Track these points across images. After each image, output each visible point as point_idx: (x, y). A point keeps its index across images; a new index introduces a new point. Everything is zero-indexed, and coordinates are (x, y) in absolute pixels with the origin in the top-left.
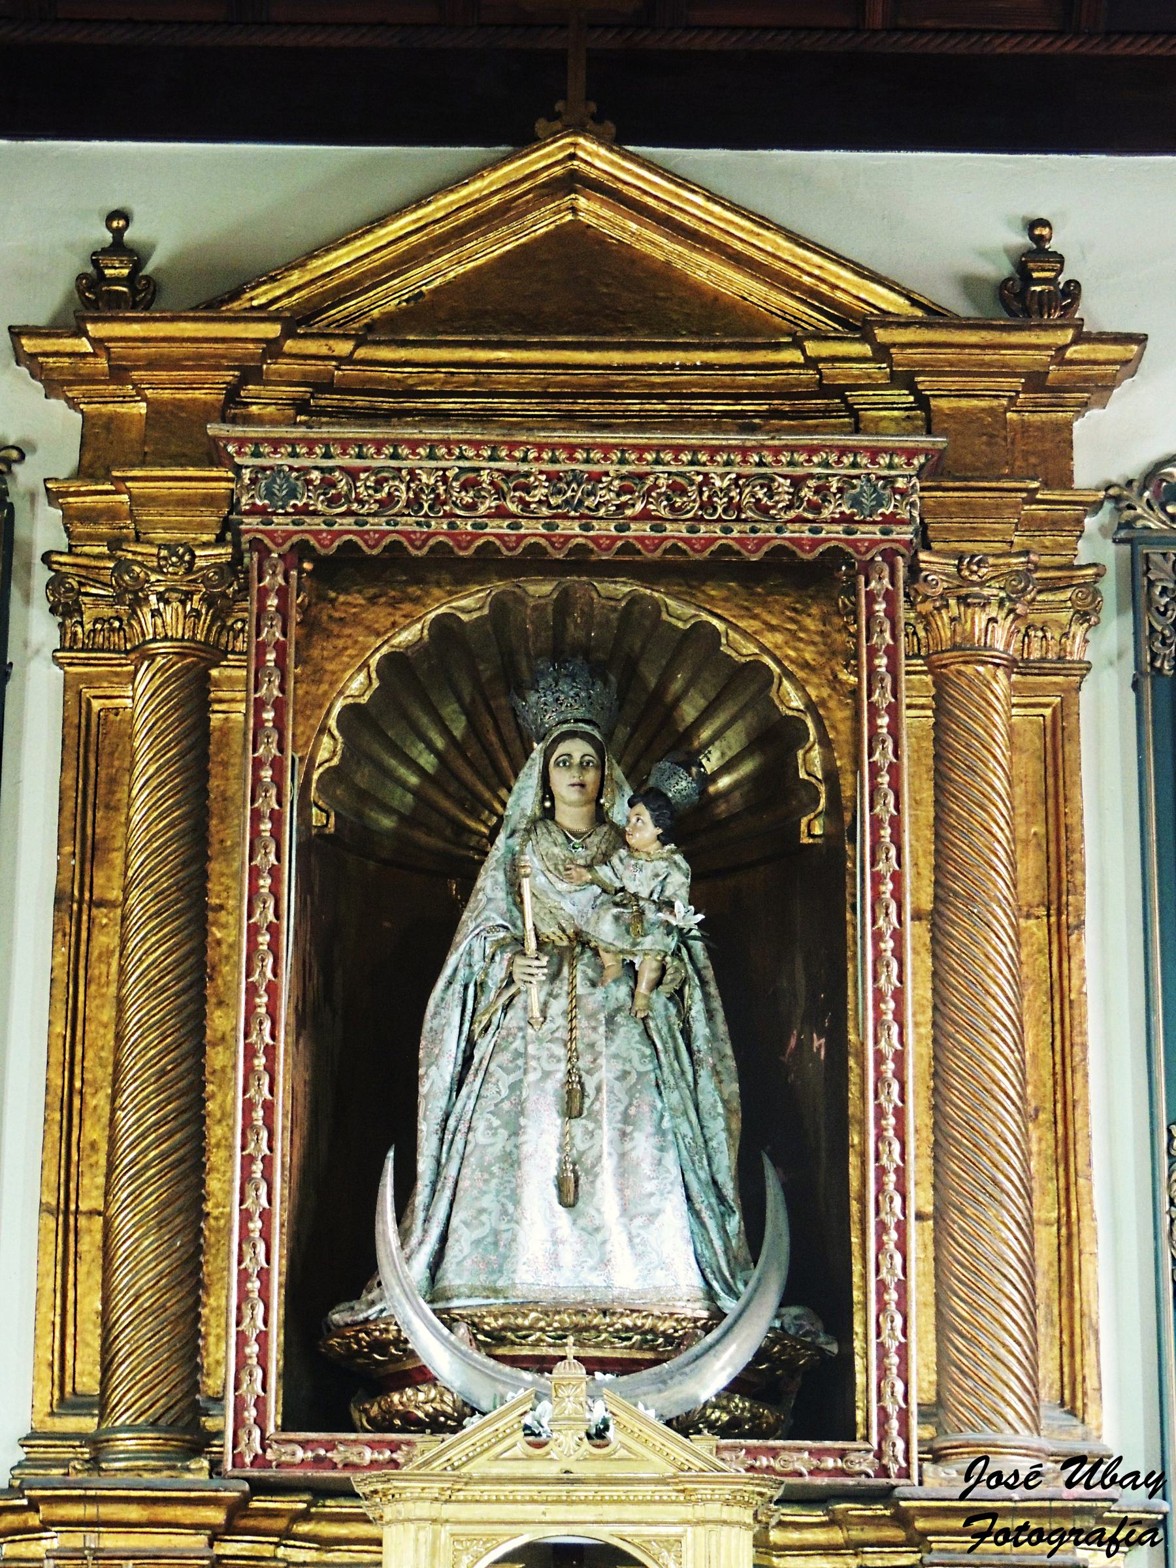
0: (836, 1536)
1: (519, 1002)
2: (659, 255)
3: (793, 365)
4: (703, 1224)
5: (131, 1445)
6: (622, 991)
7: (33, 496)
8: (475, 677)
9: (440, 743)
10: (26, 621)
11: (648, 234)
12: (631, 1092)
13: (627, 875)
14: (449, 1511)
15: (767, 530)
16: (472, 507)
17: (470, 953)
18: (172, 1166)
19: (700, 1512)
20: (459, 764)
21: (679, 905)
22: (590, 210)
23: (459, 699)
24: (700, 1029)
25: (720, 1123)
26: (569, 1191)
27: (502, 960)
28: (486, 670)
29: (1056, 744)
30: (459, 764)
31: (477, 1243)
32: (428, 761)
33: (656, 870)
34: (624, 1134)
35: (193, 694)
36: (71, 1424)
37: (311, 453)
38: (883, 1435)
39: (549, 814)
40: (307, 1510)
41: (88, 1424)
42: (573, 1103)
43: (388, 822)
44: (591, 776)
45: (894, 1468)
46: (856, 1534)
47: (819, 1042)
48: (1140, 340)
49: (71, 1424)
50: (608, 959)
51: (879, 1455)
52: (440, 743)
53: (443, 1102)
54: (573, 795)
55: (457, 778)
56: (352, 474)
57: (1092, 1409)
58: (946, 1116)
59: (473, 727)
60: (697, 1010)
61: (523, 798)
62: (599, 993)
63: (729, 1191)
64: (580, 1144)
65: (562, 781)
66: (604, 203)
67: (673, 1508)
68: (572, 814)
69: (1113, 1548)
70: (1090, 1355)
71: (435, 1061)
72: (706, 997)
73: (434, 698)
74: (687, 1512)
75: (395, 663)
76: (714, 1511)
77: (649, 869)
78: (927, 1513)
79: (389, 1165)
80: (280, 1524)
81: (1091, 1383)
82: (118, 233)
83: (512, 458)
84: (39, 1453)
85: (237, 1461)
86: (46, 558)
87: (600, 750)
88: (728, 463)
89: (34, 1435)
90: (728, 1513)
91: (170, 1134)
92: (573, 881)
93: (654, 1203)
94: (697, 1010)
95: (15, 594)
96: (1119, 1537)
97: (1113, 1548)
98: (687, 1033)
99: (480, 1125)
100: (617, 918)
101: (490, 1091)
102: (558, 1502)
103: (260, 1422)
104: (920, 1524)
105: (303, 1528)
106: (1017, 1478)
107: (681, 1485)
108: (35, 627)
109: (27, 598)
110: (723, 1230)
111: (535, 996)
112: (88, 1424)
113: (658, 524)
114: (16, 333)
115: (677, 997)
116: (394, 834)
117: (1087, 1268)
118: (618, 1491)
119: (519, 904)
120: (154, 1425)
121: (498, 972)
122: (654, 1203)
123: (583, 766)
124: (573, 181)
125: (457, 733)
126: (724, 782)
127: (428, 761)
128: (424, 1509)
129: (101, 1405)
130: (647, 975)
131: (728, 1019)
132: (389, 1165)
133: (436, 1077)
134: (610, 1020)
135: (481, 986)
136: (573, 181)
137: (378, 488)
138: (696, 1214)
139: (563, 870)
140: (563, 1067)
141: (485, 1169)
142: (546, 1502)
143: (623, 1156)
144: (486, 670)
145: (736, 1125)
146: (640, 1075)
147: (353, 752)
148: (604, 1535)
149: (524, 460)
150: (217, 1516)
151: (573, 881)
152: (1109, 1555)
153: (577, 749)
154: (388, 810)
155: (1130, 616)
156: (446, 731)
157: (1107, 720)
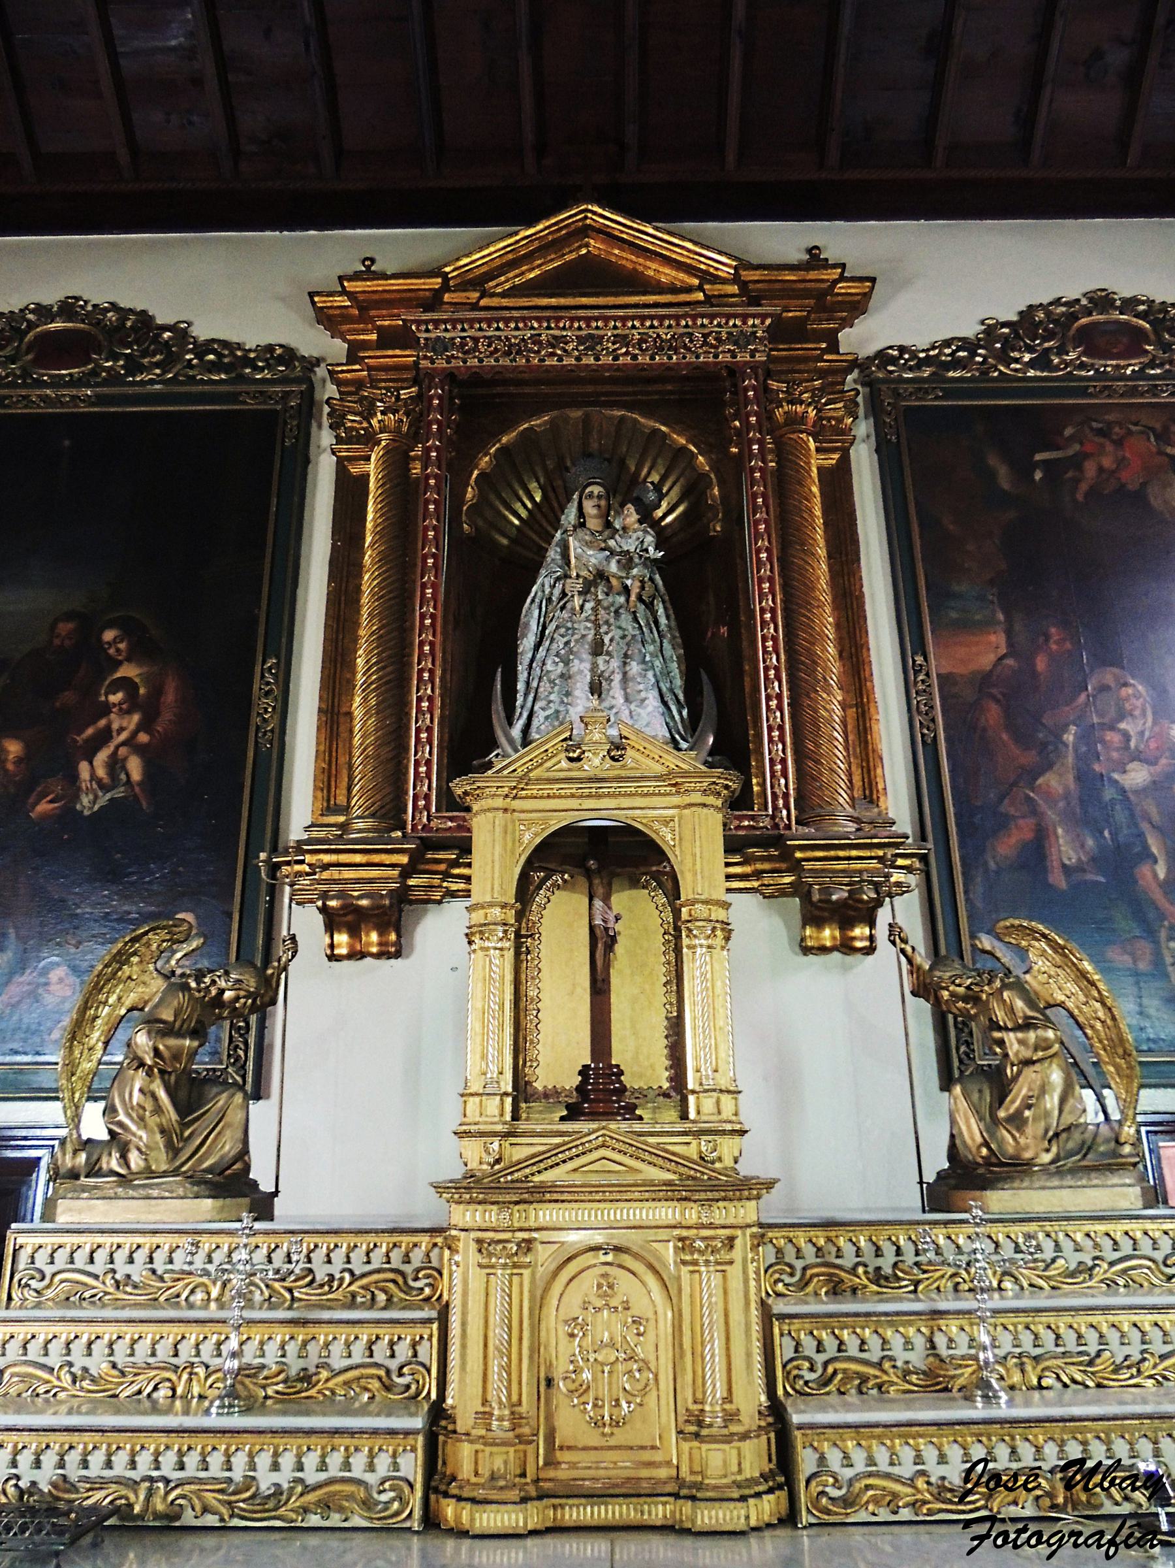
0: (748, 869)
1: (569, 606)
2: (629, 266)
3: (698, 303)
4: (669, 709)
5: (361, 825)
6: (622, 599)
7: (324, 381)
8: (545, 468)
9: (529, 505)
10: (319, 438)
11: (624, 255)
12: (628, 644)
13: (623, 542)
14: (517, 804)
15: (690, 358)
16: (538, 352)
17: (543, 585)
18: (386, 683)
19: (687, 800)
20: (539, 516)
21: (651, 549)
22: (595, 245)
23: (538, 481)
24: (663, 621)
25: (675, 665)
26: (596, 689)
27: (559, 586)
28: (550, 464)
29: (838, 483)
30: (539, 516)
31: (547, 718)
32: (524, 514)
33: (637, 538)
34: (625, 663)
35: (397, 462)
36: (332, 819)
37: (454, 328)
38: (775, 808)
39: (583, 525)
40: (456, 860)
41: (342, 819)
42: (598, 649)
43: (505, 542)
44: (603, 503)
45: (782, 825)
46: (759, 866)
47: (724, 630)
48: (873, 280)
49: (332, 819)
50: (614, 582)
51: (773, 817)
52: (529, 505)
53: (530, 655)
54: (594, 511)
55: (538, 522)
56: (476, 340)
57: (882, 799)
58: (796, 651)
59: (545, 496)
60: (661, 611)
61: (570, 516)
62: (610, 599)
63: (681, 697)
64: (602, 667)
65: (589, 507)
66: (603, 242)
67: (668, 798)
68: (593, 524)
69: (1112, 1550)
70: (879, 771)
71: (524, 635)
72: (665, 608)
73: (526, 479)
74: (676, 800)
75: (504, 450)
76: (697, 798)
77: (635, 536)
78: (802, 848)
79: (499, 675)
80: (443, 867)
81: (880, 786)
82: (368, 268)
83: (558, 328)
84: (314, 835)
85: (414, 827)
86: (327, 402)
87: (608, 493)
88: (670, 326)
89: (312, 825)
90: (711, 800)
91: (383, 668)
92: (598, 549)
93: (643, 695)
94: (661, 611)
95: (314, 425)
96: (1118, 1540)
97: (1112, 1550)
98: (656, 622)
99: (549, 662)
100: (619, 562)
101: (554, 646)
102: (590, 796)
103: (427, 807)
104: (798, 855)
105: (456, 871)
106: (1016, 1481)
107: (674, 781)
108: (325, 438)
109: (320, 426)
110: (680, 714)
111: (577, 601)
112: (342, 819)
113: (635, 357)
114: (311, 295)
115: (650, 606)
116: (508, 547)
117: (875, 727)
118: (631, 787)
119: (568, 563)
120: (372, 815)
121: (557, 592)
122: (643, 695)
123: (599, 497)
124: (585, 231)
125: (538, 499)
126: (669, 519)
127: (524, 514)
128: (499, 802)
129: (346, 809)
130: (635, 591)
131: (676, 619)
132: (499, 675)
133: (527, 643)
134: (617, 612)
135: (549, 600)
136: (585, 231)
137: (489, 345)
138: (665, 703)
139: (589, 545)
140: (593, 632)
141: (552, 682)
142: (581, 797)
143: (625, 674)
144: (550, 464)
145: (683, 668)
146: (634, 636)
147: (482, 496)
148: (625, 817)
149: (564, 328)
150: (404, 859)
151: (598, 549)
152: (1108, 1557)
153: (596, 490)
154: (505, 535)
155: (872, 420)
156: (532, 499)
157: (864, 464)
